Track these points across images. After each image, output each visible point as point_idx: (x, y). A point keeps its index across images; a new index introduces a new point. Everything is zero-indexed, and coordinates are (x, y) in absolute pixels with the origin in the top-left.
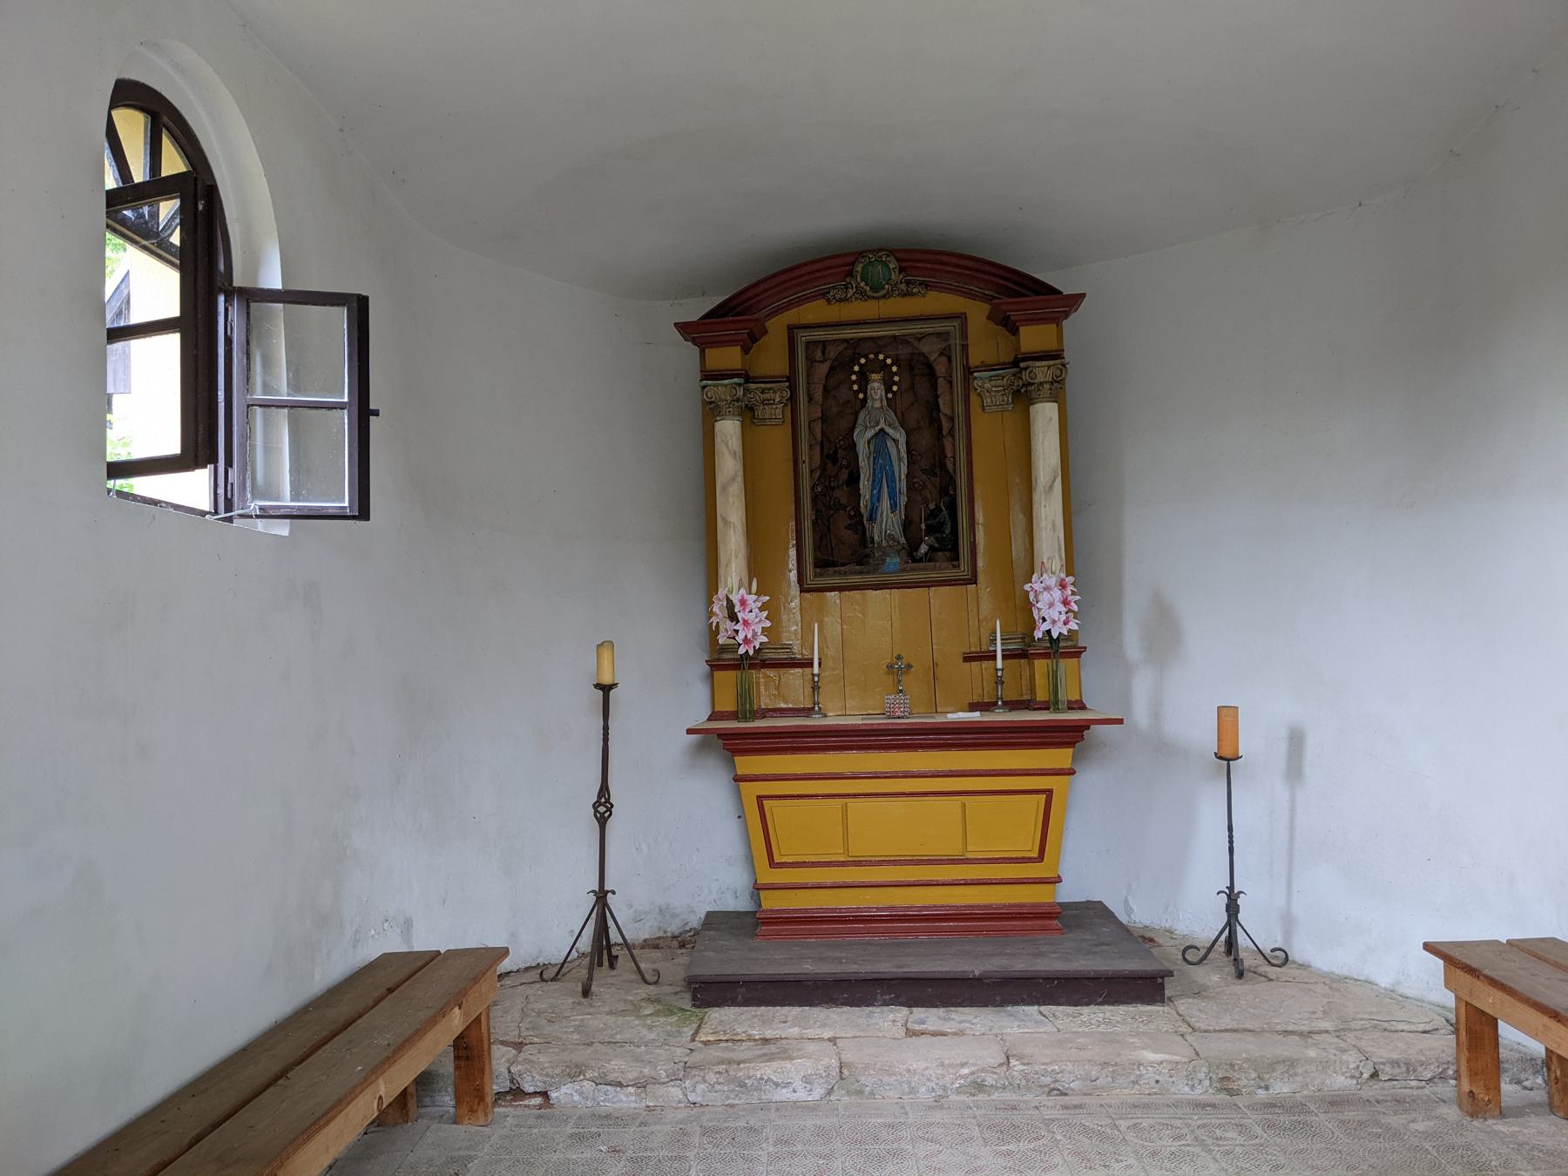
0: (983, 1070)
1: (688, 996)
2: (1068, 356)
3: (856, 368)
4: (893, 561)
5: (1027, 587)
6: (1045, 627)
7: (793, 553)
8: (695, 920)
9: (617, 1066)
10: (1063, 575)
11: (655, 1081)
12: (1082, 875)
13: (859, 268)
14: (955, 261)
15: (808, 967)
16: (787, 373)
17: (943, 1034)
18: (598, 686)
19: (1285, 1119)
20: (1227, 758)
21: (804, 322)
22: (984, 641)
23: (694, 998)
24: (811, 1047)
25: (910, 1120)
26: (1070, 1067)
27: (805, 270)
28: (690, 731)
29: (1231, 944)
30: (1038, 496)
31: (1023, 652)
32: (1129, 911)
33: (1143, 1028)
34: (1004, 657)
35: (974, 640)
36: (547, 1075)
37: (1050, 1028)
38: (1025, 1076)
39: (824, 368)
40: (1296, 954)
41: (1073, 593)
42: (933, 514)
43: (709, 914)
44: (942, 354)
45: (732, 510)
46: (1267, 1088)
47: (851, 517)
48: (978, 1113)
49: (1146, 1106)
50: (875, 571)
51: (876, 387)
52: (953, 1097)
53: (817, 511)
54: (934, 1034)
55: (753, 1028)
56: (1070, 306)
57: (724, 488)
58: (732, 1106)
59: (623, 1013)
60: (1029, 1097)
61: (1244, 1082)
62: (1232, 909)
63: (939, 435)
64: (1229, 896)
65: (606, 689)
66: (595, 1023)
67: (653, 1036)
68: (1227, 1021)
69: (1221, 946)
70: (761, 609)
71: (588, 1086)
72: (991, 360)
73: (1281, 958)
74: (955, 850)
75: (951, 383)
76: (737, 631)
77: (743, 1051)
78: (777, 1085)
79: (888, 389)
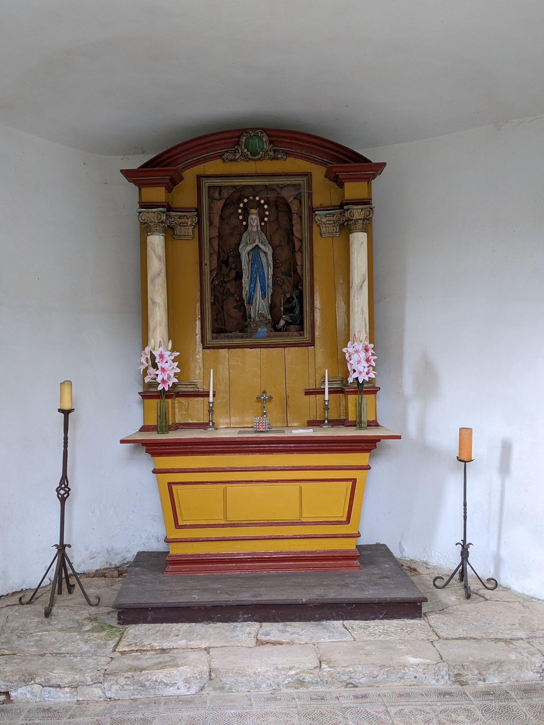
0: (304, 672)
1: (116, 615)
2: (375, 203)
3: (241, 205)
4: (263, 330)
5: (344, 350)
6: (355, 375)
7: (198, 323)
8: (130, 557)
9: (58, 674)
10: (367, 343)
11: (84, 684)
12: (373, 529)
13: (243, 140)
14: (305, 138)
15: (196, 597)
16: (196, 206)
17: (281, 643)
18: (60, 410)
19: (495, 704)
20: (464, 460)
21: (208, 173)
22: (318, 382)
23: (119, 618)
24: (193, 656)
25: (254, 711)
26: (360, 668)
27: (209, 139)
28: (122, 442)
29: (463, 575)
30: (353, 292)
31: (341, 390)
32: (402, 550)
33: (407, 637)
34: (330, 392)
35: (312, 381)
36: (9, 681)
37: (349, 638)
38: (331, 675)
39: (220, 204)
40: (502, 581)
41: (373, 355)
42: (289, 301)
43: (140, 554)
44: (295, 198)
45: (158, 295)
46: (484, 680)
47: (237, 301)
48: (299, 703)
49: (408, 695)
50: (250, 337)
51: (254, 218)
52: (284, 690)
53: (215, 296)
54: (274, 643)
55: (155, 640)
56: (377, 171)
57: (153, 280)
58: (135, 700)
59: (70, 630)
60: (333, 689)
61: (470, 677)
62: (465, 554)
63: (293, 252)
64: (463, 546)
65: (66, 413)
66: (49, 638)
67: (86, 648)
68: (460, 632)
69: (457, 576)
70: (174, 361)
71: (37, 688)
72: (327, 203)
73: (493, 584)
74: (294, 516)
75: (301, 217)
76: (157, 375)
77: (147, 660)
78: (167, 685)
79: (262, 220)
